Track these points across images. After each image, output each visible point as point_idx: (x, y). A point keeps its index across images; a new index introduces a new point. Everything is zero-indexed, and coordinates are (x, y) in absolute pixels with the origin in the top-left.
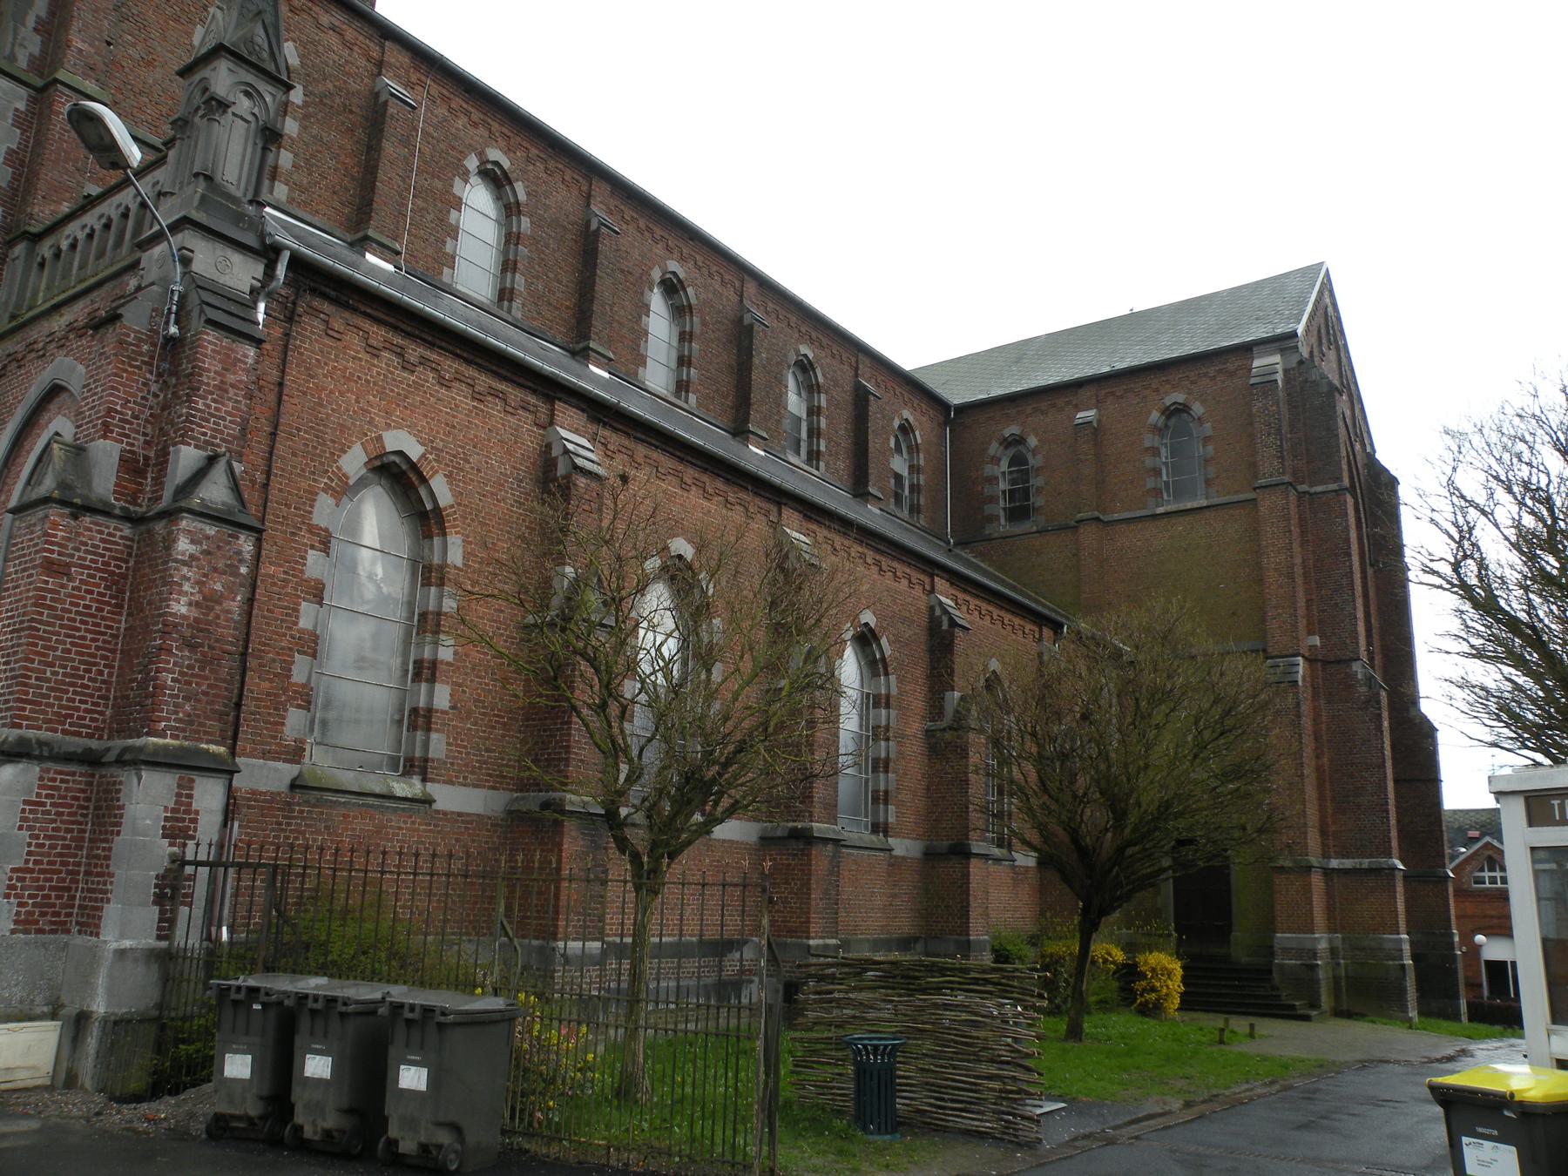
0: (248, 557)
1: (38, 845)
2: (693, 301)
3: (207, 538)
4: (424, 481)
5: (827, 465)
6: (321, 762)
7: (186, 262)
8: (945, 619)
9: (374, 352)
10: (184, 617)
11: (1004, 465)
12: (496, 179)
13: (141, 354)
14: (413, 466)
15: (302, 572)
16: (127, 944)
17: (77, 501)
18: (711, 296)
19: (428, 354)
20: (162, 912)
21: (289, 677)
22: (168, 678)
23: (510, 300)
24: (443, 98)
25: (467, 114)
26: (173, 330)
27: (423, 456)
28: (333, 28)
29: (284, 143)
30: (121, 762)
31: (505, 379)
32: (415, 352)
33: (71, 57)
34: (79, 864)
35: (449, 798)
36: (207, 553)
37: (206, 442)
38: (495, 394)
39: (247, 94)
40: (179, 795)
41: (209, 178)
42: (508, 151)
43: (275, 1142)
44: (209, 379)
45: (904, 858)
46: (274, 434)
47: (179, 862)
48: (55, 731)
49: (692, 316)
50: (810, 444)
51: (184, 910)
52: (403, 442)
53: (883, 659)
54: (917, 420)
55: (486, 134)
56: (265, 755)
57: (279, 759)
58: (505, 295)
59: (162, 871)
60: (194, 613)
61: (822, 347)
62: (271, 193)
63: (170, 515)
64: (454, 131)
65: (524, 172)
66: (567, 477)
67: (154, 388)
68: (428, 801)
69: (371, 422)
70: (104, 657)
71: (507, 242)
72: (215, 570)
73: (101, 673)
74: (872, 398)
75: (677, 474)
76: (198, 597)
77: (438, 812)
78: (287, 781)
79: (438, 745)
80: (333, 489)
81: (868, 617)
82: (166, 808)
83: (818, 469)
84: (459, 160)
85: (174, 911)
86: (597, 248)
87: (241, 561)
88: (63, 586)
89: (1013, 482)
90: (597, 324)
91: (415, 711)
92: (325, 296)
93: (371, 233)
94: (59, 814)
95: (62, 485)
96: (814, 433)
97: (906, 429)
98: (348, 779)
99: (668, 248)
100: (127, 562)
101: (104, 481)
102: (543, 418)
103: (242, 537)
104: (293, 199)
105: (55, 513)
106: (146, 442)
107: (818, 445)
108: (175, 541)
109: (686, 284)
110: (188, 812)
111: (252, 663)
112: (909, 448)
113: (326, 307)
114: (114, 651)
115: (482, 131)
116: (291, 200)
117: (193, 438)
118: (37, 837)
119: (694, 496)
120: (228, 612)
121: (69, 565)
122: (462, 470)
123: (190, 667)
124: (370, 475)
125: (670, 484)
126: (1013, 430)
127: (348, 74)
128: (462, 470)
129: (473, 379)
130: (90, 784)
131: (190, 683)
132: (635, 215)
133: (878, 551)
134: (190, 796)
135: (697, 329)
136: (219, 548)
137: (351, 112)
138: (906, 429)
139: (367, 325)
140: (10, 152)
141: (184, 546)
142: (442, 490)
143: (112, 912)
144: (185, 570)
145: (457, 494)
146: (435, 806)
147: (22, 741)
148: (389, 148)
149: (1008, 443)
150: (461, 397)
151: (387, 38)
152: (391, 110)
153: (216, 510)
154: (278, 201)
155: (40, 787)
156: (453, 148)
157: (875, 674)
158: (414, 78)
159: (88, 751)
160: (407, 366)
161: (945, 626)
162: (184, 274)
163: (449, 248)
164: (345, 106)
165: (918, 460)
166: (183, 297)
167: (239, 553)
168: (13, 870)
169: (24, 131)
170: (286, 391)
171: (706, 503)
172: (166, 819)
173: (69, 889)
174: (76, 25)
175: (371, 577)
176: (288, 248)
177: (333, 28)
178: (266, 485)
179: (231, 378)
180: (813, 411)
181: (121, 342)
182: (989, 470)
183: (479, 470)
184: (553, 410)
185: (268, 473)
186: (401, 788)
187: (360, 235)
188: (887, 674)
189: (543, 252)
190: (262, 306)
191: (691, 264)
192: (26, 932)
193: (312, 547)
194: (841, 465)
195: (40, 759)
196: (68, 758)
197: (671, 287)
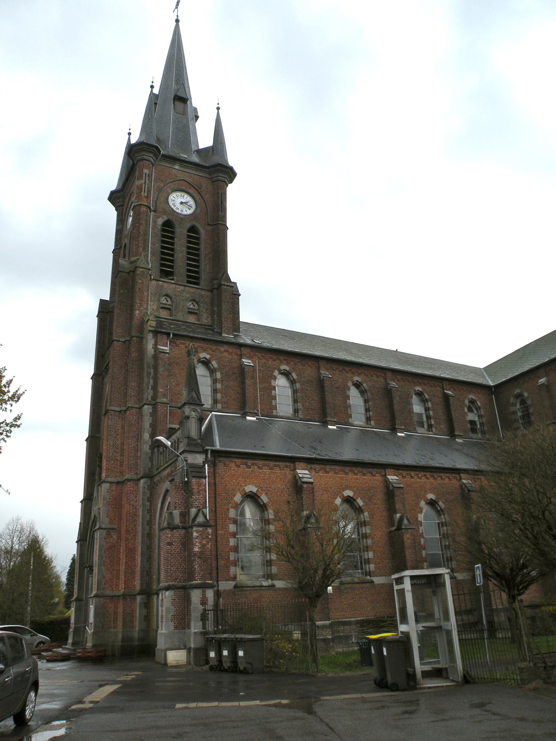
0: (210, 533)
1: (176, 609)
2: (367, 388)
3: (200, 531)
4: (259, 497)
5: (436, 429)
6: (242, 578)
7: (186, 461)
8: (466, 489)
9: (238, 466)
10: (198, 551)
11: (518, 406)
12: (286, 374)
13: (180, 487)
14: (255, 494)
15: (229, 531)
16: (196, 631)
17: (172, 527)
18: (373, 383)
19: (254, 461)
20: (203, 623)
21: (229, 559)
22: (196, 567)
23: (298, 413)
24: (262, 356)
25: (272, 358)
26: (186, 479)
27: (257, 490)
28: (225, 351)
29: (218, 392)
30: (189, 588)
31: (278, 461)
32: (250, 462)
33: (160, 394)
34: (185, 613)
35: (279, 584)
36: (200, 535)
37: (197, 506)
38: (276, 466)
39: (194, 411)
40: (203, 594)
41: (188, 438)
42: (288, 364)
43: (235, 672)
44: (195, 490)
45: (463, 580)
46: (215, 497)
47: (205, 610)
48: (175, 582)
49: (367, 393)
50: (428, 422)
51: (207, 622)
52: (251, 488)
53: (441, 509)
54: (476, 397)
55: (279, 362)
56: (226, 580)
57: (230, 581)
58: (296, 411)
59: (201, 613)
60: (200, 550)
61: (425, 385)
62: (217, 408)
63: (191, 527)
64: (268, 365)
65: (294, 368)
66: (301, 485)
67: (185, 494)
68: (273, 586)
69: (241, 486)
70: (184, 563)
71: (294, 393)
72: (203, 538)
73: (183, 566)
74: (450, 397)
75: (342, 470)
76: (200, 546)
77: (277, 588)
78: (233, 586)
79: (274, 569)
80: (233, 506)
81: (430, 496)
82: (200, 598)
83: (432, 431)
84: (272, 374)
85: (206, 622)
86: (324, 385)
87: (209, 535)
88: (172, 548)
89: (523, 412)
90: (329, 411)
91: (267, 561)
92: (222, 457)
93: (247, 410)
94: (179, 601)
95: (168, 524)
96: (429, 418)
97: (472, 402)
98: (250, 583)
99: (353, 373)
100: (185, 538)
101: (177, 520)
102: (293, 468)
103: (208, 529)
104: (223, 407)
105: (168, 531)
106: (185, 508)
107: (431, 422)
108: (193, 533)
109: (362, 383)
110: (206, 598)
111: (219, 557)
112: (477, 409)
113: (223, 459)
114: (185, 561)
115: (278, 361)
116: (223, 407)
117: (194, 506)
118: (175, 607)
119: (351, 475)
120: (208, 548)
121: (172, 542)
122: (269, 491)
123: (201, 563)
124: (245, 499)
125: (341, 474)
126: (517, 391)
127: (232, 362)
128: (269, 491)
129: (269, 464)
130: (185, 593)
131: (201, 567)
132: (338, 367)
133: (431, 472)
134: (205, 594)
135: (370, 398)
136: (203, 533)
137: (235, 373)
138: (472, 402)
139: (235, 460)
140: (150, 424)
141: (195, 534)
142: (264, 498)
143: (192, 623)
144: (196, 540)
145: (269, 498)
146: (276, 587)
147: (169, 585)
148: (248, 382)
149: (518, 396)
150: (266, 471)
151: (241, 347)
152: (246, 370)
153: (201, 524)
154: (219, 409)
155: (175, 595)
156: (269, 371)
157: (440, 515)
158: (252, 355)
159: (183, 586)
160: (249, 467)
161: (467, 492)
162: (187, 464)
163: (274, 404)
164: (233, 372)
165: (481, 413)
166: (187, 470)
167: (208, 533)
168: (172, 615)
169: (152, 417)
170: (217, 484)
171: (355, 476)
172: (201, 600)
173: (184, 619)
174: (159, 385)
175: (250, 525)
176: (209, 449)
177: (225, 351)
178: (216, 511)
179: (200, 488)
180: (427, 410)
181: (175, 485)
182: (512, 409)
183: (275, 489)
184: (295, 465)
185: (216, 508)
186: (265, 584)
187: (244, 411)
188: (444, 515)
189: (306, 392)
190: (206, 465)
191: (363, 375)
192: (177, 629)
193: (230, 524)
194: (443, 426)
195: (173, 589)
196: (179, 588)
197: (358, 385)
